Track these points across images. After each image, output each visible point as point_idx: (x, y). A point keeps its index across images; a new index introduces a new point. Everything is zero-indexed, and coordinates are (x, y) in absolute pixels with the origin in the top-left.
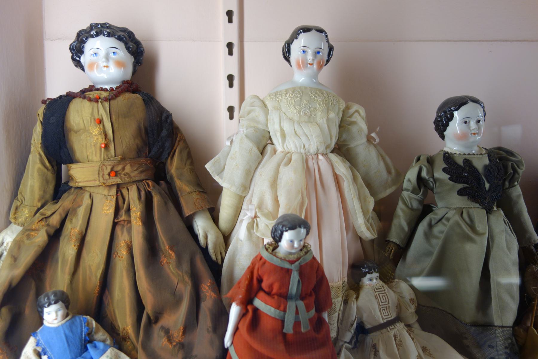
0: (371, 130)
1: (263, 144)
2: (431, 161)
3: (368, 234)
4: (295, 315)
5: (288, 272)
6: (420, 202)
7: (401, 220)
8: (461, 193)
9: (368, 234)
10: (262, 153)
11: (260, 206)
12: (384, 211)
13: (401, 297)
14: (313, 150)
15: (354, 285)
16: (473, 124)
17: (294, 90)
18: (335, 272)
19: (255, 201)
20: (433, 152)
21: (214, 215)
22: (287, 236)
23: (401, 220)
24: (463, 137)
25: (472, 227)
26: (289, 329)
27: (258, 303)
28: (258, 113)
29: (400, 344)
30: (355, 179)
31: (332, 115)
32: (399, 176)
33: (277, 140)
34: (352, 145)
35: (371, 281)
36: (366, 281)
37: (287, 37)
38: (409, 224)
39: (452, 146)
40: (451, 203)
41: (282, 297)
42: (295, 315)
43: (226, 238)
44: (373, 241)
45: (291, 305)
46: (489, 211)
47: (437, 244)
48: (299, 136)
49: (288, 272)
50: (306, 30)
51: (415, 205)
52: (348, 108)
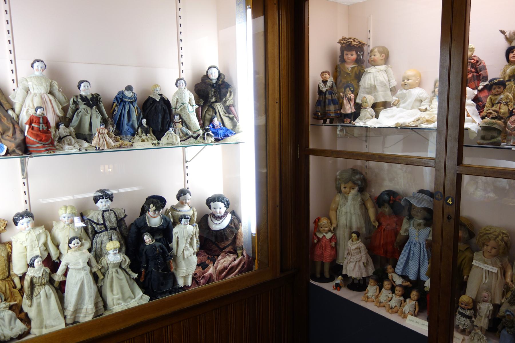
0: (59, 87)
1: (27, 91)
2: (77, 97)
3: (60, 115)
4: (42, 127)
5: (40, 118)
6: (75, 107)
7: (70, 112)
8: (84, 104)
9: (60, 115)
10: (27, 93)
11: (29, 106)
12: (65, 110)
13: (71, 131)
14: (43, 92)
15: (57, 127)
16: (86, 87)
17: (36, 77)
18: (52, 122)
19: (27, 105)
20: (78, 94)
21: (13, 109)
22: (39, 110)
23: (70, 112)
24: (84, 91)
25: (87, 112)
26: (41, 129)
27: (33, 125)
28: (25, 82)
29: (70, 140)
30: (56, 101)
31: (47, 84)
32: (69, 100)
33: (31, 90)
34: (54, 92)
35: (62, 126)
36: (61, 126)
37: (32, 62)
38: (72, 113)
39: (83, 93)
40: (82, 106)
41: (39, 123)
42: (42, 127)
43: (18, 116)
44: (62, 117)
45: (41, 125)
46: (91, 108)
47: (79, 117)
48: (38, 89)
49: (40, 118)
50: (38, 61)
51: (74, 108)
52: (52, 82)
